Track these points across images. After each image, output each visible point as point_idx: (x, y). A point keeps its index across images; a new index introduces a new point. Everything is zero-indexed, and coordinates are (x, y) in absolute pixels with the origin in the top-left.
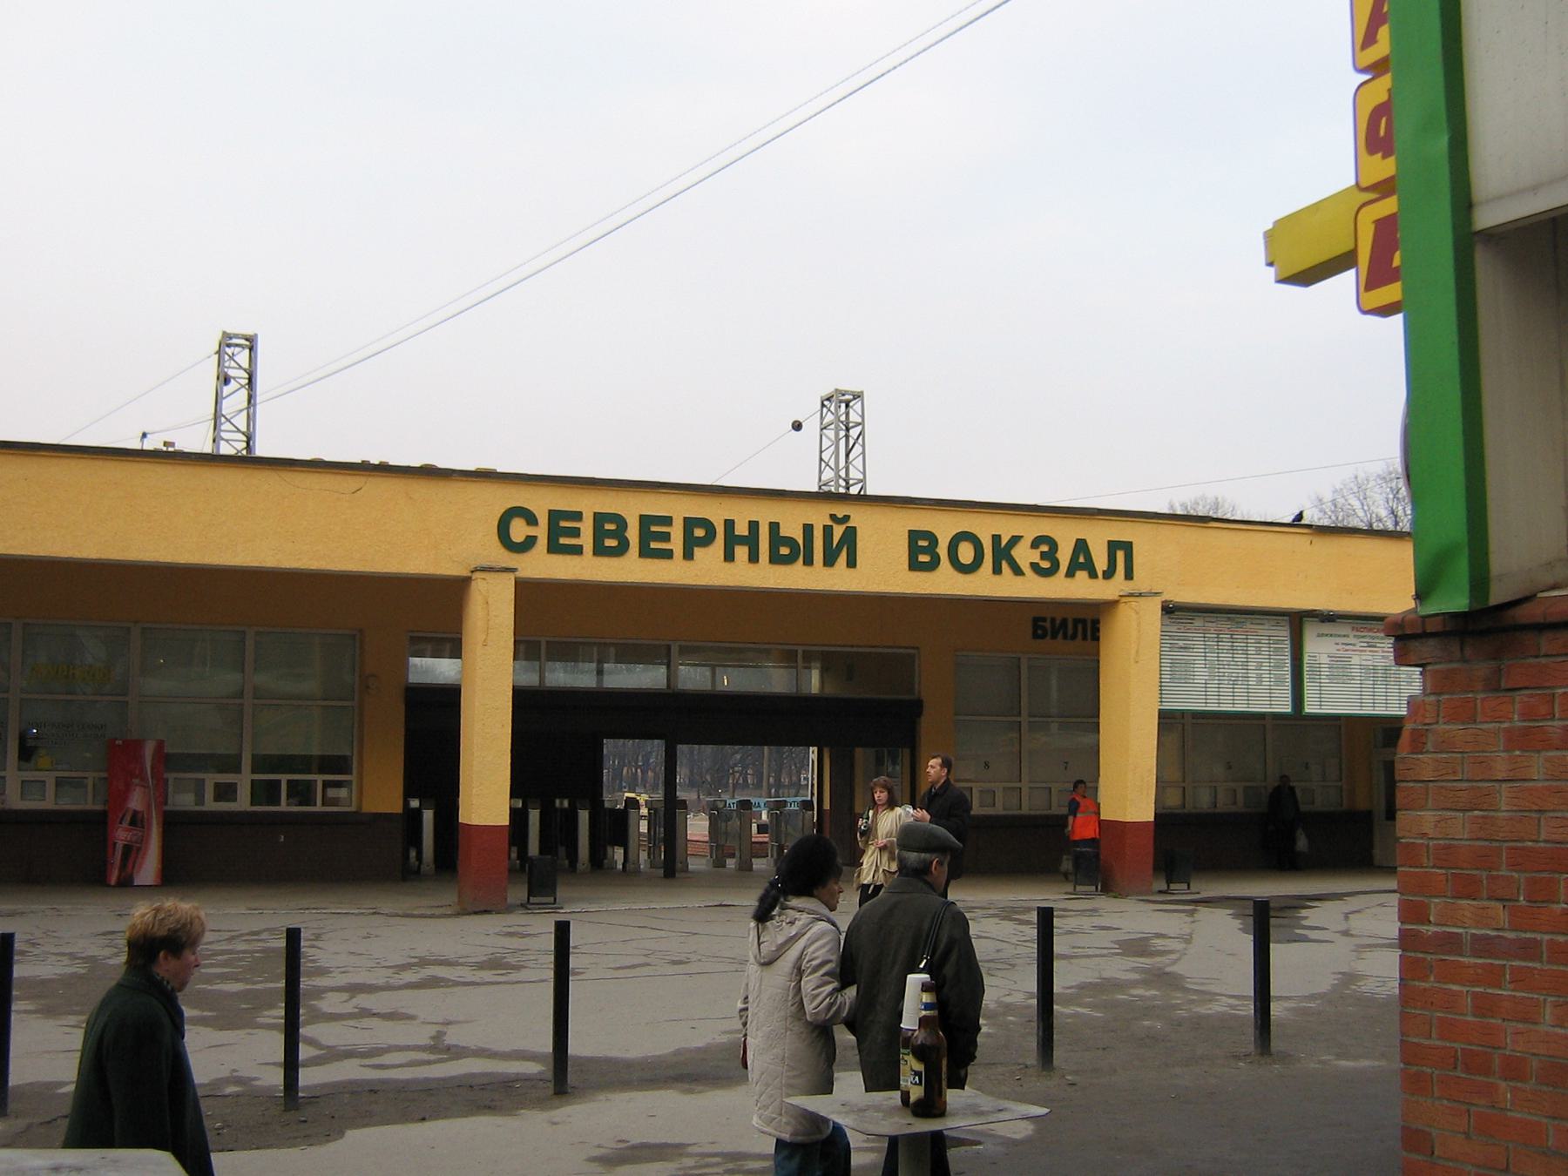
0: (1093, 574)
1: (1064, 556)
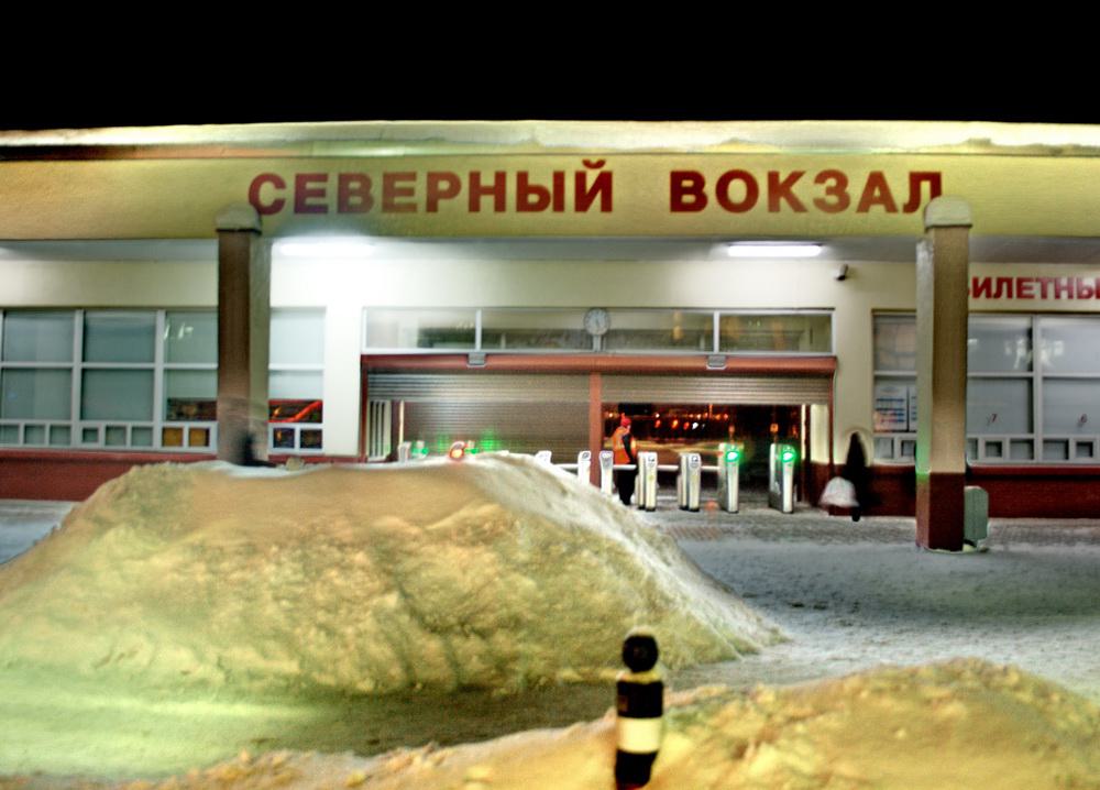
0: (891, 208)
1: (856, 189)
